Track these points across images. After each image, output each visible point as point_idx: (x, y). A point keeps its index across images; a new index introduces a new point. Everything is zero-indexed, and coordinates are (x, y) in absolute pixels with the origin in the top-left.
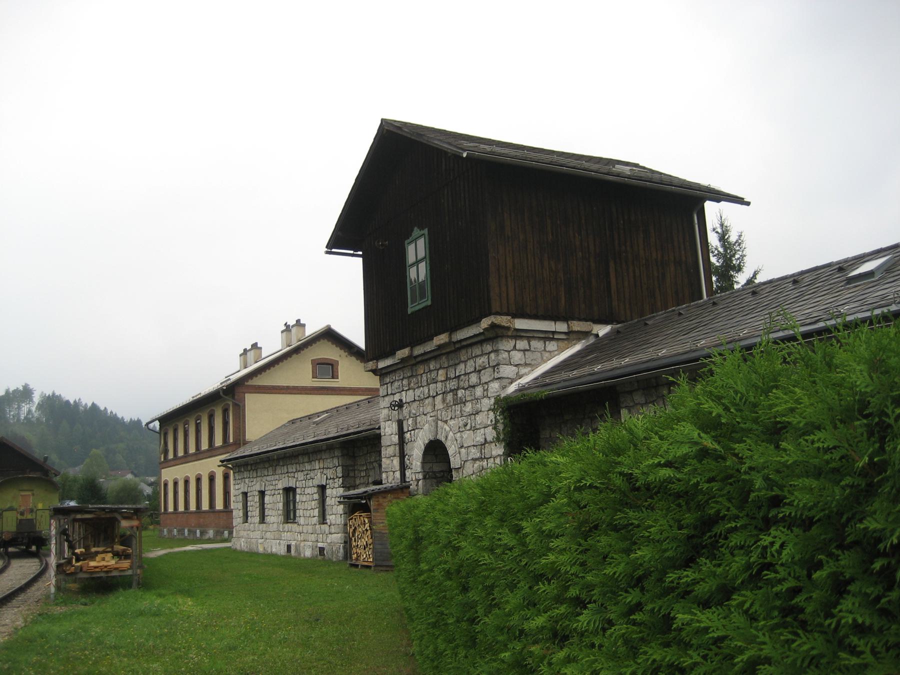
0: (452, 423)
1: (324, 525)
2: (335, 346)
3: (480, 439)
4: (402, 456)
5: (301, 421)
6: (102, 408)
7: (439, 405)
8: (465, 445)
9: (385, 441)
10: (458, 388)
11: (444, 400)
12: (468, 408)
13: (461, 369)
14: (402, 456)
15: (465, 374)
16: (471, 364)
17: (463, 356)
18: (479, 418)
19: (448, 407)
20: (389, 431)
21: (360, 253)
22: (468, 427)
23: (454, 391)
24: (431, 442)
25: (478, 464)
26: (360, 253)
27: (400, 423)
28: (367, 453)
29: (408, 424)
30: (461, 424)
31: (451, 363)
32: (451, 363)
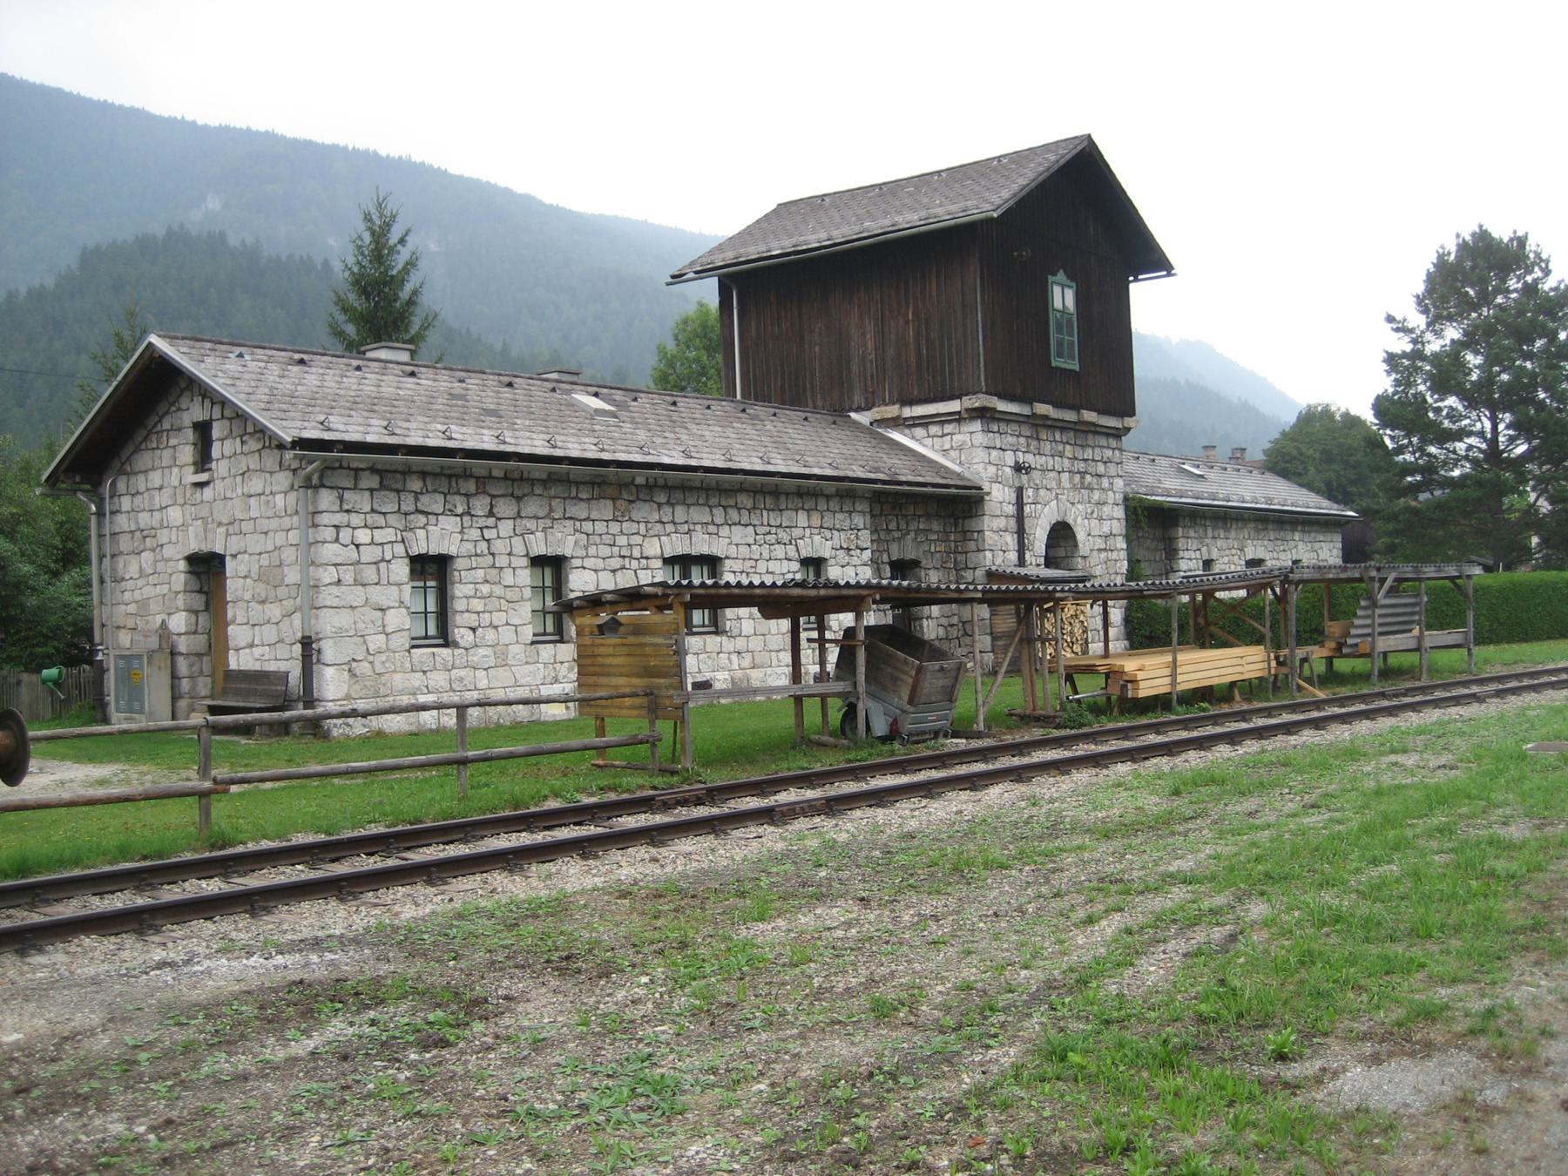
0: (1080, 506)
1: (718, 639)
2: (199, 123)
3: (1106, 530)
4: (1021, 532)
5: (554, 390)
6: (179, 118)
7: (1066, 483)
8: (249, 551)
9: (991, 506)
10: (1086, 472)
11: (1071, 480)
12: (1096, 495)
13: (1088, 453)
14: (1021, 532)
15: (1093, 460)
16: (1098, 454)
17: (1091, 439)
18: (1106, 510)
19: (1074, 488)
20: (999, 497)
21: (1063, 298)
22: (1095, 515)
23: (1083, 474)
24: (1058, 523)
25: (1103, 555)
26: (1063, 298)
27: (1020, 492)
28: (881, 515)
29: (1029, 494)
30: (1089, 511)
31: (1079, 442)
32: (1079, 442)
